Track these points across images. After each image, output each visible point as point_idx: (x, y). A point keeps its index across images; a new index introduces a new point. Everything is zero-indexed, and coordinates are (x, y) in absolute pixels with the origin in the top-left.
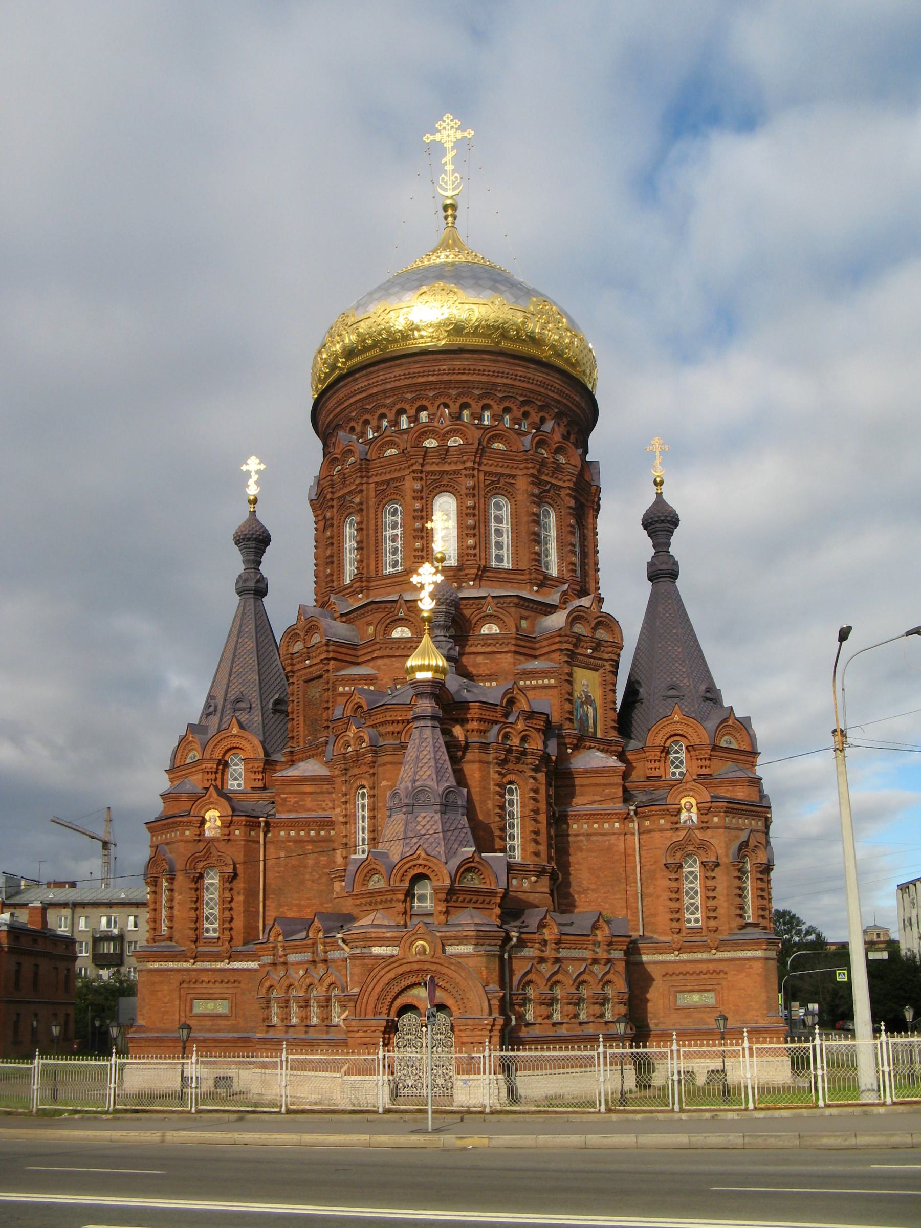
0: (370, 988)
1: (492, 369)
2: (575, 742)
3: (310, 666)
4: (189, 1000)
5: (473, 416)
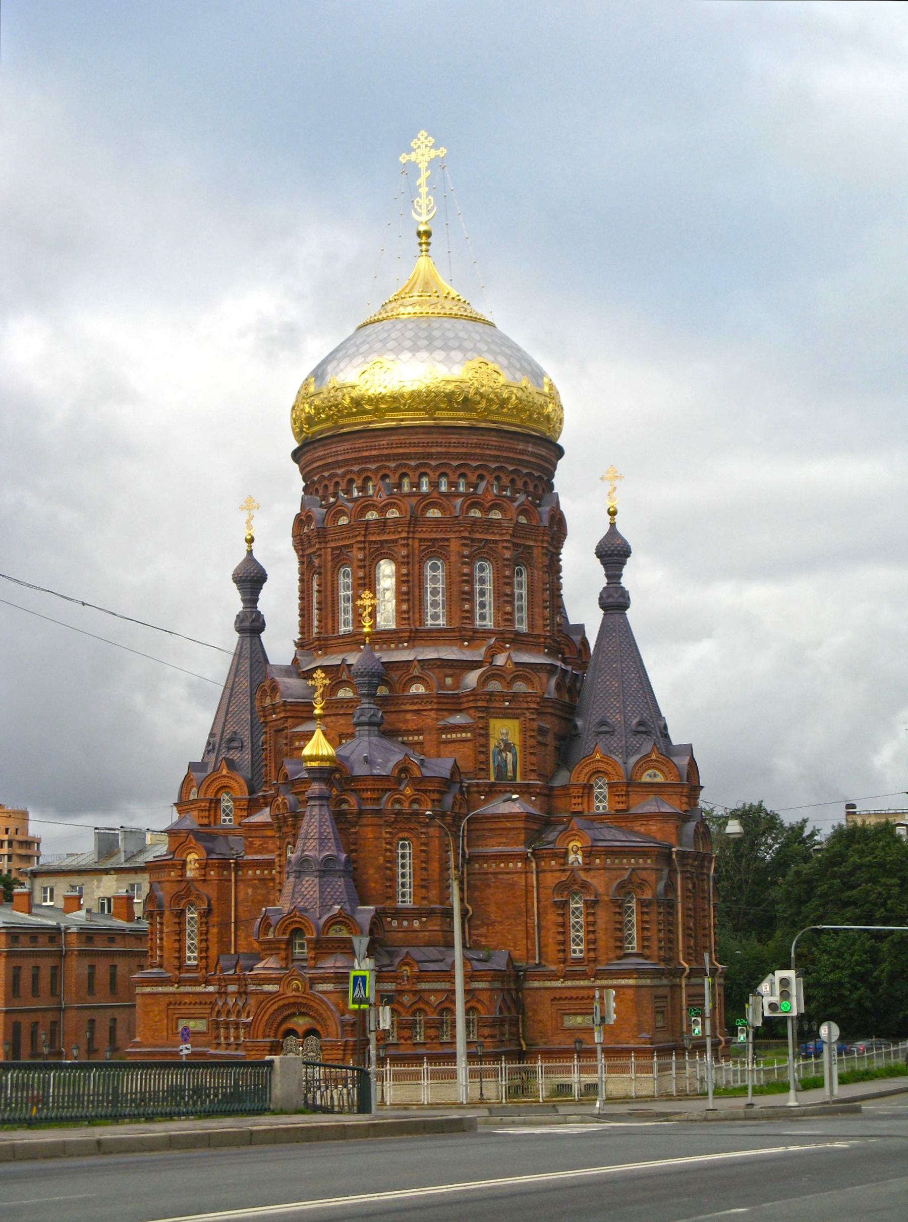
0: (260, 1017)
1: (426, 441)
2: (487, 789)
3: (276, 720)
4: (175, 1020)
5: (412, 485)
